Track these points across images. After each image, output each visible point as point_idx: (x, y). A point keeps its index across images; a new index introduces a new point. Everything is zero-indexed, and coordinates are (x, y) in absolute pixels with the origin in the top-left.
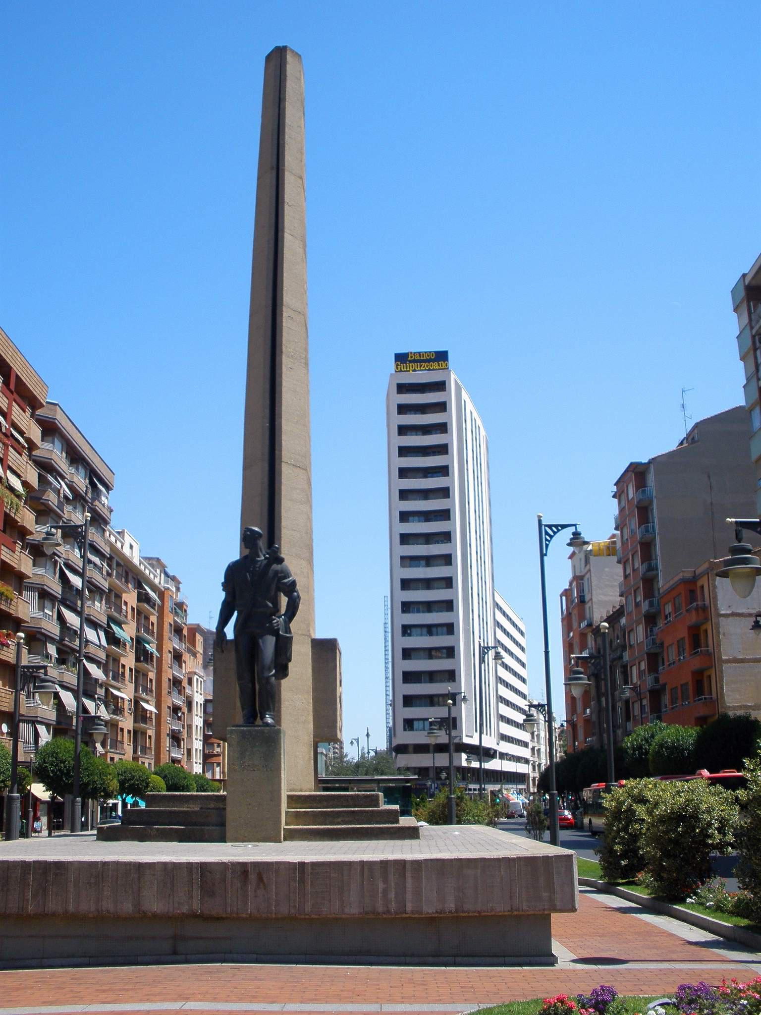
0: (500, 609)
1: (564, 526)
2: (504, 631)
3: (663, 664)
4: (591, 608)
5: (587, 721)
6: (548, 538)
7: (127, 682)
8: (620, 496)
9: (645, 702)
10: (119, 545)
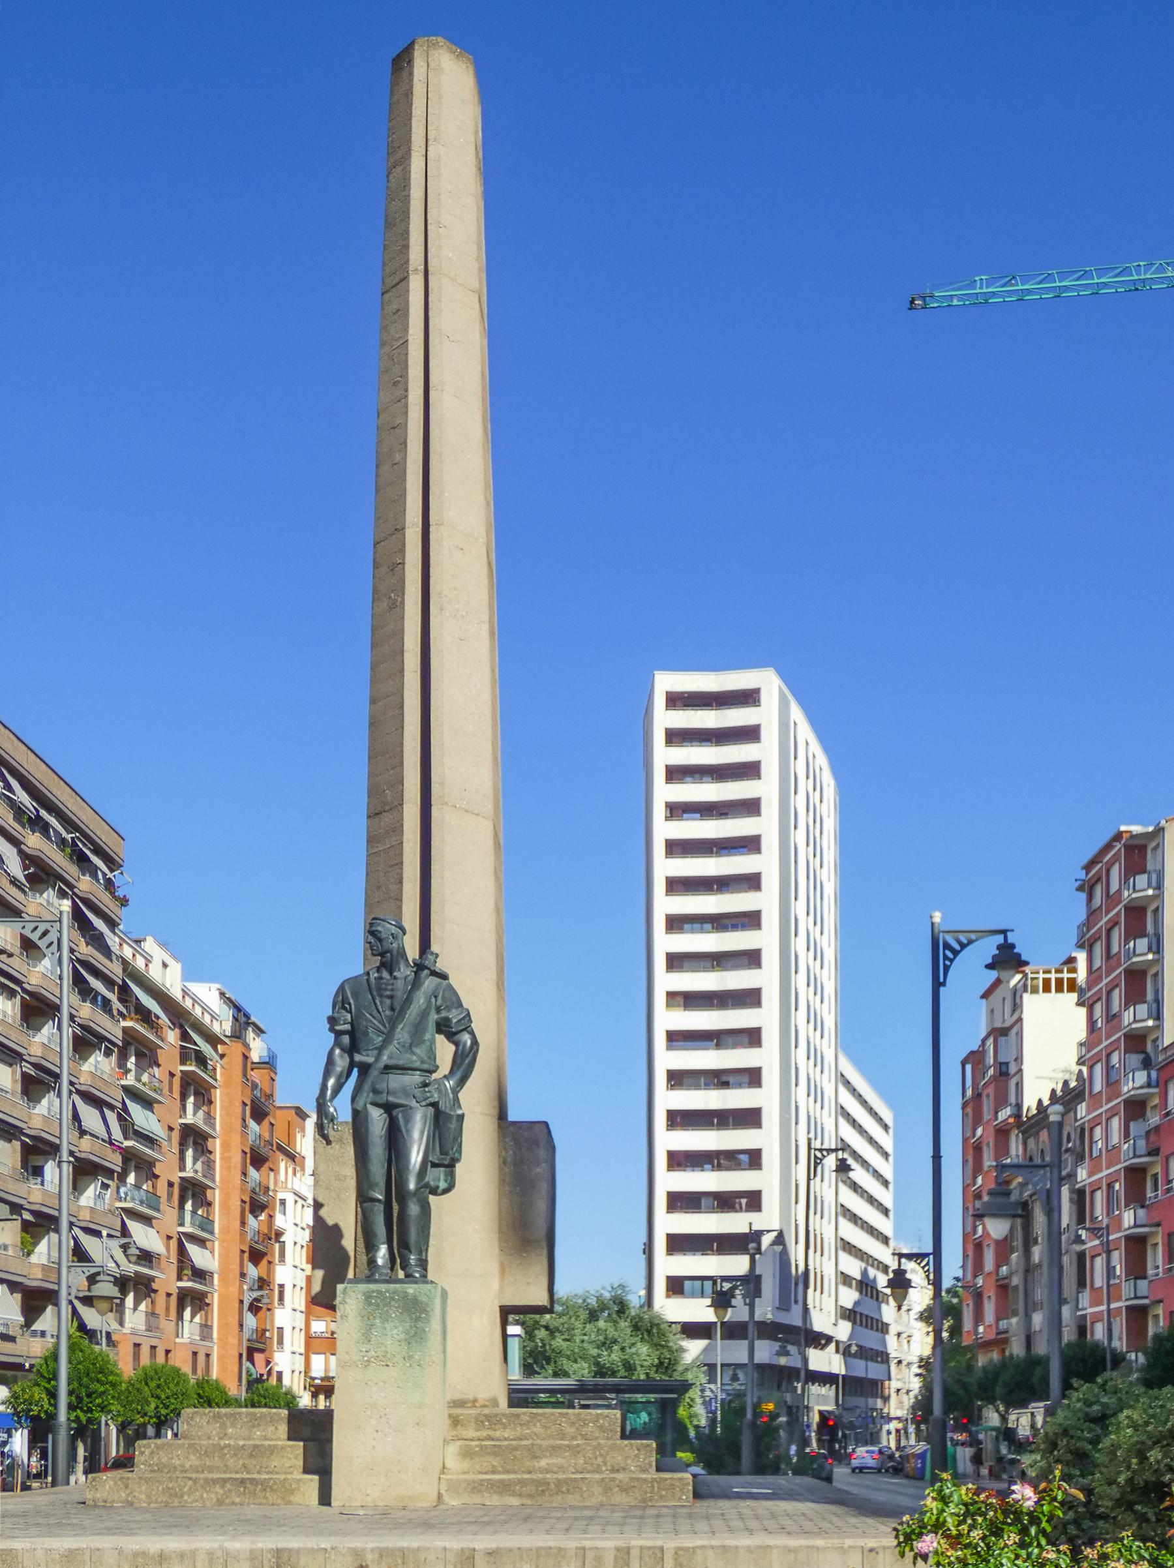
0: (847, 1083)
1: (768, 1231)
2: (854, 1123)
3: (1156, 1190)
4: (1019, 1086)
6: (950, 955)
7: (164, 1205)
9: (1116, 1255)
10: (140, 963)
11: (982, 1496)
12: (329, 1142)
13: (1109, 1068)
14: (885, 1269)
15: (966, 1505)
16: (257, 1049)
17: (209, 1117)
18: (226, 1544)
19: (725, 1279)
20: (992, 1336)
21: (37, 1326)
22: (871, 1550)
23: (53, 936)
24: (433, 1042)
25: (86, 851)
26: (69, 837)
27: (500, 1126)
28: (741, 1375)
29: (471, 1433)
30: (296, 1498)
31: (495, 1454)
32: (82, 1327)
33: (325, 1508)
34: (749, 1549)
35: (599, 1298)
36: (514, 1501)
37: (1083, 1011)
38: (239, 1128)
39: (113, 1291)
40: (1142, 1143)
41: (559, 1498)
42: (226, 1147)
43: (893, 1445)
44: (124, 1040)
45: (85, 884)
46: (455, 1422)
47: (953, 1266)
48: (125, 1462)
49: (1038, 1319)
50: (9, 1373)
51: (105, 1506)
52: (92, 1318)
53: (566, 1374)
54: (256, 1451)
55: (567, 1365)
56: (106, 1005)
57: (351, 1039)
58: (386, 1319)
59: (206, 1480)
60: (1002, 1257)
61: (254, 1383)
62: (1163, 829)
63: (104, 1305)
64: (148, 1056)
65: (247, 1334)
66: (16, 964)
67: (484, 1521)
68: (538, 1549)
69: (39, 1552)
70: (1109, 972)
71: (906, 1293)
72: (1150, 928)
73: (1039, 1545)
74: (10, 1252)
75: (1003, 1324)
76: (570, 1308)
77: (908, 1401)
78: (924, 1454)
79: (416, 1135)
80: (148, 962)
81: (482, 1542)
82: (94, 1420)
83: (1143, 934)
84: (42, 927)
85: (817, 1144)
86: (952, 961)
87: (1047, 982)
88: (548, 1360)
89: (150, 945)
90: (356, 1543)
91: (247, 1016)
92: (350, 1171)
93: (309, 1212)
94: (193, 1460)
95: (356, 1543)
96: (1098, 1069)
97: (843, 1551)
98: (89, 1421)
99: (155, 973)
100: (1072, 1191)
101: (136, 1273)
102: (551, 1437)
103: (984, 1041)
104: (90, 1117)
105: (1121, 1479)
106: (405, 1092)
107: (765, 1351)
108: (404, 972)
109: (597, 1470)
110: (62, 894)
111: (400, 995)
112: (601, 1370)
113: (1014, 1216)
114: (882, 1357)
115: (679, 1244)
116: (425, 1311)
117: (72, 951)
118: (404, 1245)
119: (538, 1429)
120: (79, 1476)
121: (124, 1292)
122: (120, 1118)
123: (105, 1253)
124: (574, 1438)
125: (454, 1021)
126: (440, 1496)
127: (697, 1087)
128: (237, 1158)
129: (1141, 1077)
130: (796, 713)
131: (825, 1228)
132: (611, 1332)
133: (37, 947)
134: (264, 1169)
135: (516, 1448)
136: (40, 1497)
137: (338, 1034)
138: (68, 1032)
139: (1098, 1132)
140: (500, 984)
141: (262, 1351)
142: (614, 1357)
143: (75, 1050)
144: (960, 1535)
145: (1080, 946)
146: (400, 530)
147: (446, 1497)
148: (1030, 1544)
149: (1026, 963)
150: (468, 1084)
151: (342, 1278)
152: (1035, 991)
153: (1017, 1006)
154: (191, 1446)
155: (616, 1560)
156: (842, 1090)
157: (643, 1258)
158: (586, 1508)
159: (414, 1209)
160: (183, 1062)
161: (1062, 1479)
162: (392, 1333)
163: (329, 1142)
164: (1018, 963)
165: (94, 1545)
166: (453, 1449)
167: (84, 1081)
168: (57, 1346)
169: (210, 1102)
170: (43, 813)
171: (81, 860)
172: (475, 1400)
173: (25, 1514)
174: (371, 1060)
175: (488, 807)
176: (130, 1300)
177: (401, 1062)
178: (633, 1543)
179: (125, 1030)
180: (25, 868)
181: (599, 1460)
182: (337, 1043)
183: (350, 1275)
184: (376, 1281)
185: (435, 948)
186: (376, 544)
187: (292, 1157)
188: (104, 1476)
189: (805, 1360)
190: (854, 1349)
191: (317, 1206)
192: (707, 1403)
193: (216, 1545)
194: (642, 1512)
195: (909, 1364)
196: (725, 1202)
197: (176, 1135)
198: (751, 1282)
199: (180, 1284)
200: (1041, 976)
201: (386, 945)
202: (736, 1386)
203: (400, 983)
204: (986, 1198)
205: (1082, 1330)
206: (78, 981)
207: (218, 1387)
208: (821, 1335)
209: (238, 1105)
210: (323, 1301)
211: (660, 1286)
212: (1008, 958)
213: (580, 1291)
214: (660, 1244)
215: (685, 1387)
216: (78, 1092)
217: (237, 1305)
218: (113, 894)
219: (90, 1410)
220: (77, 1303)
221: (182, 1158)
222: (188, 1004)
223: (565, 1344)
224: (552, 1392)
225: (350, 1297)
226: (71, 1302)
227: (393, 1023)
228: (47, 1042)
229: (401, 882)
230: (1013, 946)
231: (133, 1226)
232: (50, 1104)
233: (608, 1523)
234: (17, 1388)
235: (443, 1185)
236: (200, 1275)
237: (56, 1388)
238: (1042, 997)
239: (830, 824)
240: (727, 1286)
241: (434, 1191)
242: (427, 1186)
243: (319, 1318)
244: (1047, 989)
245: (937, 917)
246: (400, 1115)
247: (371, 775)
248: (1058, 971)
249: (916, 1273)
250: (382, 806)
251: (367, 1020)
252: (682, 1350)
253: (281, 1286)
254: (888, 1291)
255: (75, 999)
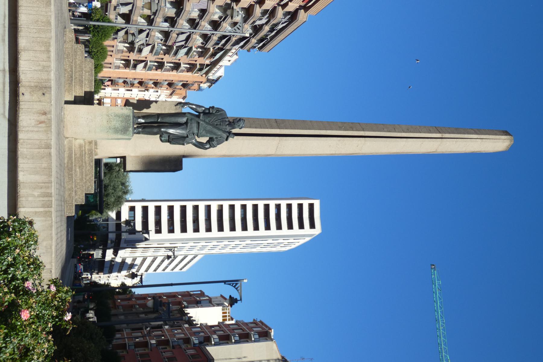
0: (194, 257)
2: (182, 260)
5: (132, 306)
7: (156, 57)
8: (255, 323)
9: (142, 339)
10: (230, 54)
11: (68, 304)
12: (176, 105)
13: (199, 332)
14: (138, 271)
15: (65, 299)
16: (204, 86)
17: (182, 71)
18: (53, 72)
19: (134, 224)
20: (117, 304)
21: (119, 17)
22: (51, 271)
23: (238, 31)
24: (207, 136)
25: (264, 42)
26: (268, 37)
27: (181, 156)
28: (105, 229)
29: (87, 147)
30: (67, 94)
31: (80, 155)
32: (118, 31)
33: (64, 102)
34: (51, 234)
35: (128, 186)
36: (66, 161)
37: (217, 324)
38: (180, 80)
39: (130, 40)
40: (176, 344)
41: (67, 175)
42: (174, 76)
43: (83, 276)
44: (206, 48)
45: (254, 41)
46: (90, 143)
47: (138, 291)
48: (77, 41)
49: (122, 317)
50: (104, 8)
51: (64, 35)
52: (122, 33)
53: (105, 176)
54: (81, 82)
55: (108, 177)
56: (217, 44)
57: (208, 112)
58: (122, 121)
59: (72, 66)
60: (141, 306)
61: (102, 82)
63: (125, 37)
64: (202, 54)
65: (117, 79)
66: (229, 20)
67: (60, 152)
68: (51, 169)
69: (50, 14)
70: (229, 330)
71: (130, 278)
72: (242, 340)
73: (52, 322)
74: (141, 11)
75: (121, 307)
76: (125, 177)
77: (97, 280)
78: (81, 286)
79: (178, 131)
80: (231, 56)
81: (53, 151)
82: (91, 31)
83: (240, 338)
84: (241, 28)
85: (176, 249)
87: (226, 313)
88: (109, 171)
89: (235, 57)
90: (53, 112)
91: (214, 83)
92: (167, 112)
93: (154, 99)
94: (78, 62)
95: (53, 112)
96: (199, 329)
97: (51, 262)
98: (90, 31)
99: (227, 58)
100: (162, 325)
101: (135, 48)
102: (86, 172)
103: (207, 296)
104: (183, 37)
105: (73, 345)
106: (191, 128)
107: (112, 236)
108: (228, 128)
109: (75, 187)
110: (251, 34)
111: (221, 127)
112: (106, 187)
113: (154, 308)
114: (110, 272)
115: (145, 209)
116: (124, 133)
117: (233, 36)
118: (144, 127)
119: (88, 168)
120: (73, 27)
121: (129, 43)
122: (182, 46)
123: (141, 39)
124: (85, 179)
126: (67, 138)
127: (193, 214)
128: (171, 79)
129: (196, 342)
130: (308, 239)
131: (150, 253)
132: (118, 190)
133: (235, 26)
134: (167, 86)
135: (82, 161)
136: (67, 15)
137: (209, 109)
138: (209, 33)
139: (180, 331)
140: (224, 156)
141: (112, 84)
142: (110, 191)
143: (203, 34)
144: (56, 298)
145: (236, 321)
146: (363, 130)
147: (67, 140)
148: (53, 319)
149: (231, 307)
150: (194, 147)
151: (134, 108)
152: (223, 310)
153: (218, 305)
154: (83, 61)
155: (48, 193)
156: (193, 256)
157: (141, 199)
158: (64, 183)
159: (155, 130)
160: (200, 64)
161: (73, 328)
162: (117, 124)
163: (176, 105)
164: (231, 305)
165: (52, 30)
166: (82, 142)
167: (194, 36)
168: (113, 23)
169: (188, 72)
170: (275, 31)
171: (261, 40)
172: (97, 149)
173: (61, 10)
174: (201, 118)
175: (279, 153)
176: (127, 45)
177: (200, 127)
178: (53, 198)
179: (209, 49)
180: (259, 25)
181: (79, 187)
182: (206, 109)
183: (135, 111)
184: (133, 119)
185: (236, 137)
186: (359, 124)
187: (171, 94)
188: (73, 34)
189: (109, 249)
190: (113, 263)
191: (156, 102)
192: (96, 219)
193: (52, 68)
194: (62, 200)
195: (108, 280)
196: (158, 223)
197: (177, 61)
198: (133, 231)
199: (132, 61)
200: (227, 311)
201: (236, 123)
202: (102, 228)
204: (159, 300)
205: (119, 331)
206: (224, 37)
207: (101, 70)
208: (117, 253)
209: (187, 80)
210: (127, 103)
211: (132, 204)
212: (233, 301)
213: (130, 180)
214: (145, 204)
215: (101, 212)
216: (190, 35)
217: (126, 77)
218: (251, 48)
219: (93, 31)
220: (126, 29)
221: (170, 63)
222: (218, 67)
223: (114, 176)
224: (100, 172)
225: (128, 111)
226: (126, 28)
227: (212, 125)
228: (205, 26)
229: (256, 128)
230: (237, 302)
231: (149, 47)
232: (187, 26)
233: (59, 190)
234: (100, 10)
235: (163, 139)
236: (135, 66)
237: (100, 21)
238: (221, 312)
239: (274, 250)
240: (132, 224)
241: (161, 136)
242: (163, 134)
243: (122, 101)
244: (223, 313)
245: (245, 281)
247: (288, 120)
248: (229, 316)
249: (136, 280)
250: (278, 124)
252: (112, 211)
253: (131, 90)
254: (131, 272)
255: (219, 35)
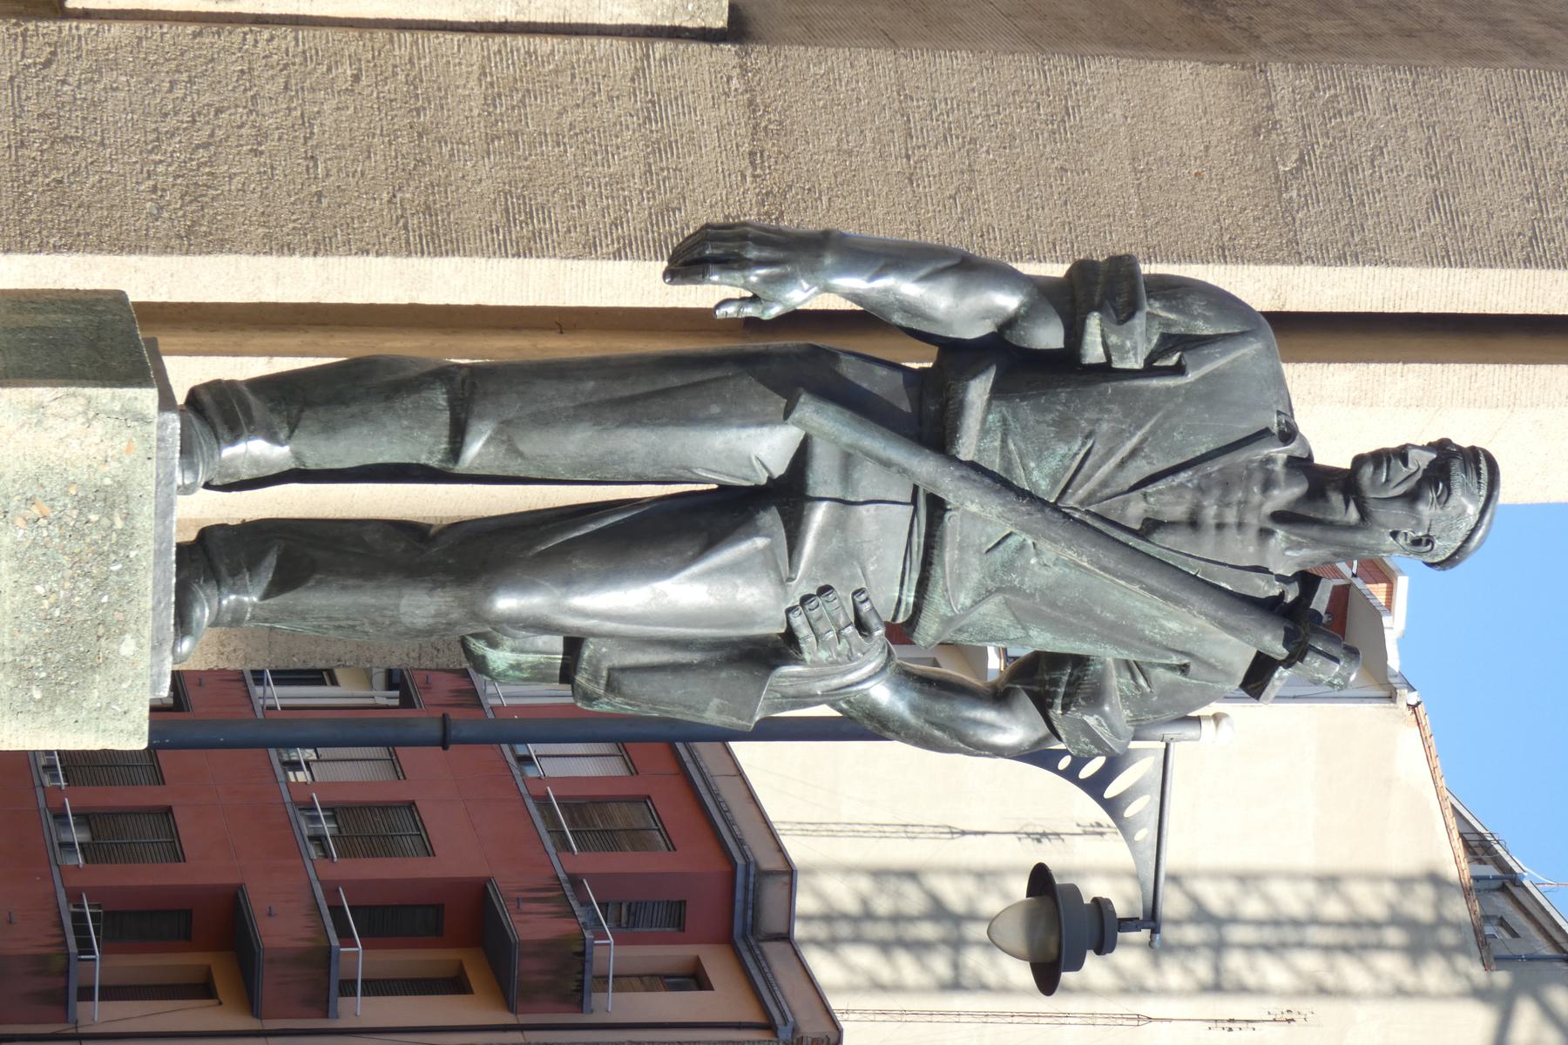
62: (1392, 697)
86: (1071, 774)
116: (53, 697)
125: (1091, 720)
174: (967, 448)
177: (949, 555)
203: (1243, 549)
227: (1095, 527)
246: (760, 542)
251: (1119, 436)
